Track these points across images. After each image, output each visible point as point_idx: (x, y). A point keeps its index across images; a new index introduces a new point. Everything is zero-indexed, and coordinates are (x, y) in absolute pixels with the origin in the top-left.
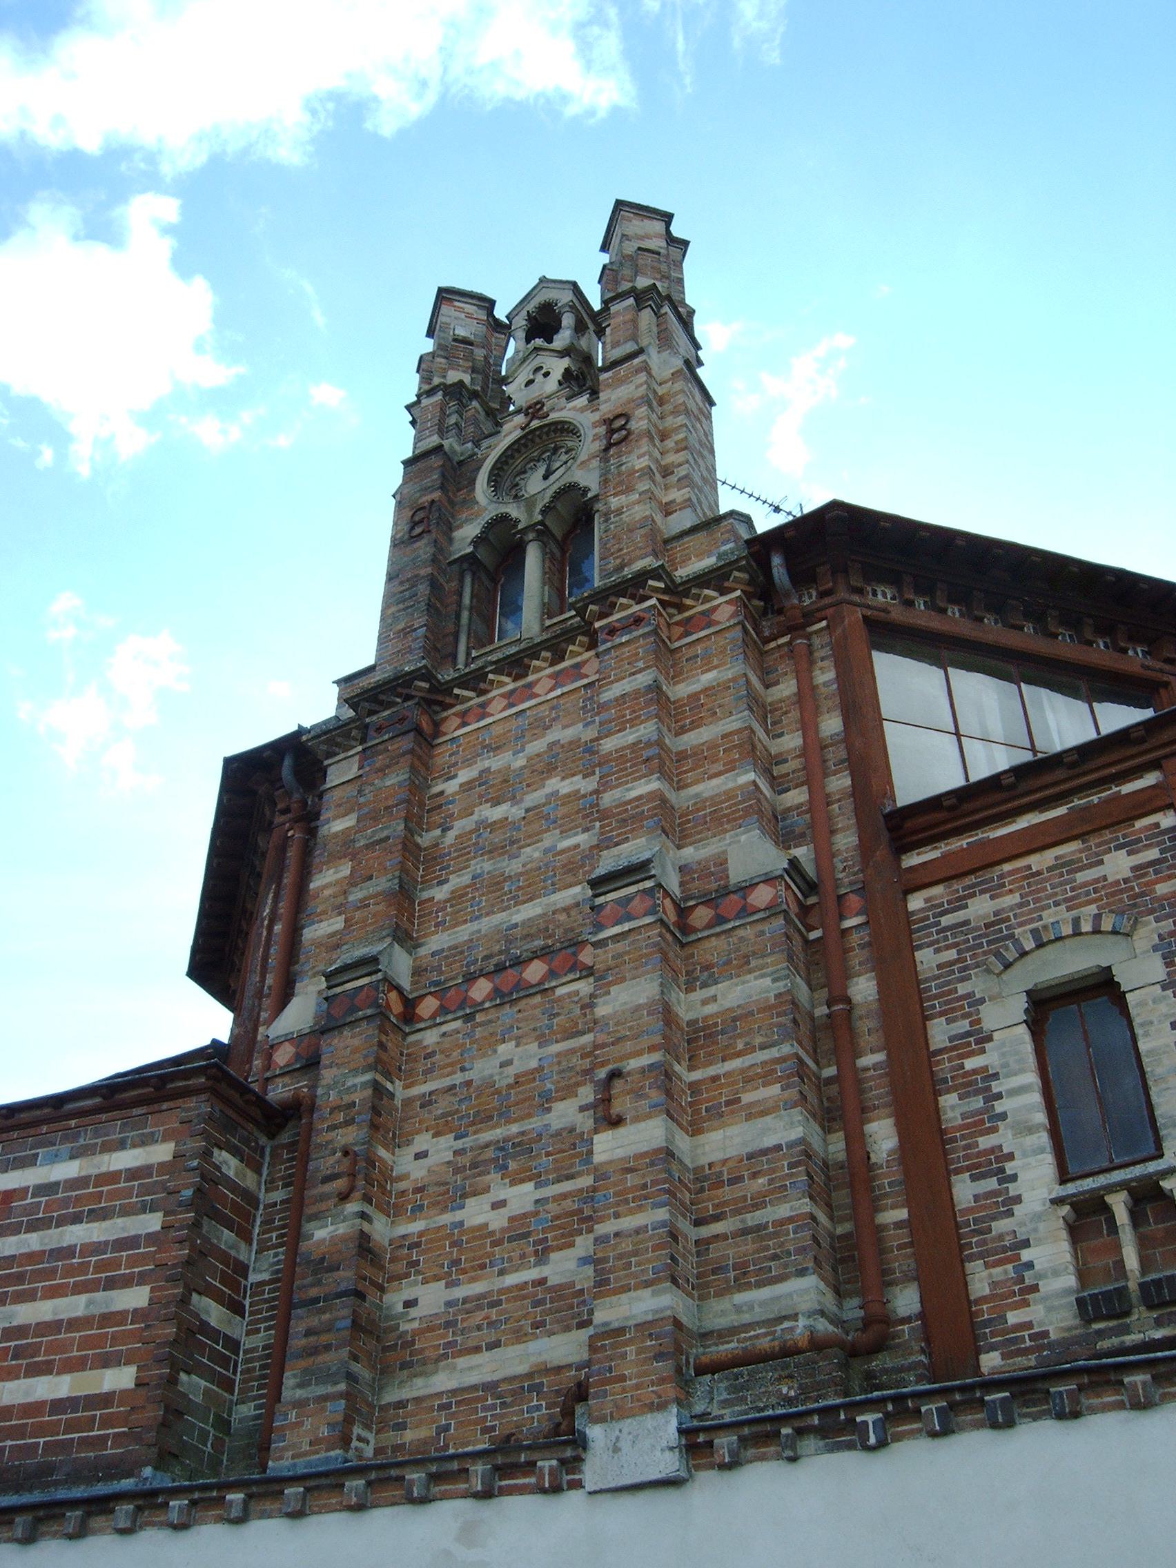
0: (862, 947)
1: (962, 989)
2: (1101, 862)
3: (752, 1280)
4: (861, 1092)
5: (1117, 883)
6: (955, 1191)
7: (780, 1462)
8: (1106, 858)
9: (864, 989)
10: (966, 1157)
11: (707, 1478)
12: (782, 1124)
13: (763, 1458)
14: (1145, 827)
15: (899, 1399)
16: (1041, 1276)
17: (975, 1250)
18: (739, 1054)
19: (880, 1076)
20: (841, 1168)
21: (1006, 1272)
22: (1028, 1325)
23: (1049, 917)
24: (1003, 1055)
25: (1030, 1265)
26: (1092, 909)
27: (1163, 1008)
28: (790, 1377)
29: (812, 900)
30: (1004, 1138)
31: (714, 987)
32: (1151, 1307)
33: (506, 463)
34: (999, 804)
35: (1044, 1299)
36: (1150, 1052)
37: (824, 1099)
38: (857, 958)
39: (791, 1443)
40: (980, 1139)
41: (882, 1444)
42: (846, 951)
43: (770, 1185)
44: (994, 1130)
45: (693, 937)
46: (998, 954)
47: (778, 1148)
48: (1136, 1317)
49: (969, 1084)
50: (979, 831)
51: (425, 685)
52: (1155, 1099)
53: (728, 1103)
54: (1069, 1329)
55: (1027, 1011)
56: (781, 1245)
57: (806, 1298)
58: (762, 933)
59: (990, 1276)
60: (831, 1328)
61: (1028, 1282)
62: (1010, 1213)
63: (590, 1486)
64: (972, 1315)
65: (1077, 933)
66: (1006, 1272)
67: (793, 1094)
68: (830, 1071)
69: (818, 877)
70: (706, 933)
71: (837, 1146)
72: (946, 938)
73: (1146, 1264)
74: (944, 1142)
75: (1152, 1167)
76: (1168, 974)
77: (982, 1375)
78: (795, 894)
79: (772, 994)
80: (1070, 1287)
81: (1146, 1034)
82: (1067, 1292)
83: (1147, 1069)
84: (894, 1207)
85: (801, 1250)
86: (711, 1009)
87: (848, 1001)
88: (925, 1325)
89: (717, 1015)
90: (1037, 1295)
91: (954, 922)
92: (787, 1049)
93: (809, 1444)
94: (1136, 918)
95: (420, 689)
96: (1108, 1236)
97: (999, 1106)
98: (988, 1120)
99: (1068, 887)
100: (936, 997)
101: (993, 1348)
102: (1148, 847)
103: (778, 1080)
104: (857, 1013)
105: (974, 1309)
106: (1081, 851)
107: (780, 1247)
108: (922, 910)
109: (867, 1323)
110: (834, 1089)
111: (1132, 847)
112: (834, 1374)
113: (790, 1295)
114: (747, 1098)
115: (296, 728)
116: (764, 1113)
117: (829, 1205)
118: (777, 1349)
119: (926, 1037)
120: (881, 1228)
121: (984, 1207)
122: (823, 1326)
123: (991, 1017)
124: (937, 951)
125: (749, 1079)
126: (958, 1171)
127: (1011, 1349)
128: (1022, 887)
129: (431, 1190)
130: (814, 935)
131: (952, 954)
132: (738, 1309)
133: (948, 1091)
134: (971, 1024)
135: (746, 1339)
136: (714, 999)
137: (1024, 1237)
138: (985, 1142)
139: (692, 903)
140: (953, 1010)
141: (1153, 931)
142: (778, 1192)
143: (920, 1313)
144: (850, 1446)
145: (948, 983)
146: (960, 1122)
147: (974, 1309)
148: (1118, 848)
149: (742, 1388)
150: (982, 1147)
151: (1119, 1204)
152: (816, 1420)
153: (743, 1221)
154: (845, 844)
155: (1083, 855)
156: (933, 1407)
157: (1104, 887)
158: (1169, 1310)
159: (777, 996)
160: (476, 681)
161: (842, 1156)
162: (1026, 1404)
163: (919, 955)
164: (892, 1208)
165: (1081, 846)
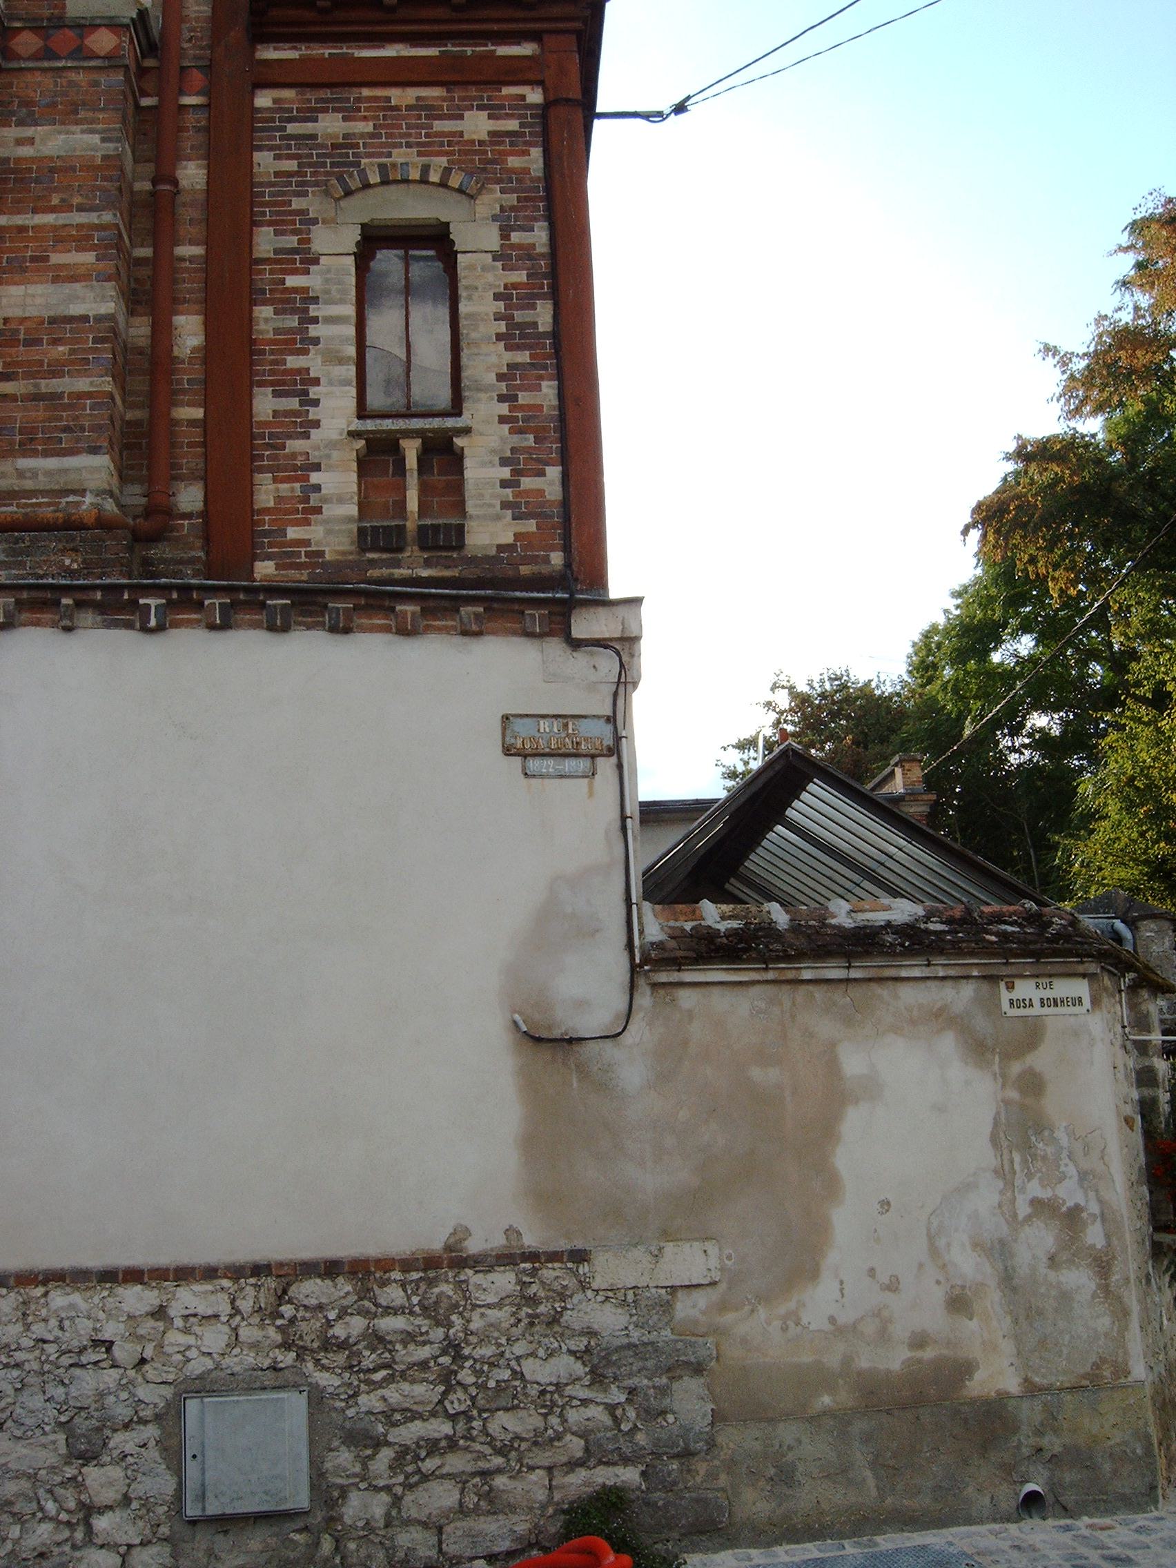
0: (198, 130)
1: (296, 204)
2: (461, 117)
3: (40, 448)
4: (175, 281)
5: (473, 142)
6: (255, 402)
7: (55, 629)
8: (467, 114)
9: (192, 174)
10: (272, 372)
12: (92, 295)
13: (37, 624)
14: (511, 95)
15: (187, 589)
16: (326, 500)
17: (265, 463)
18: (53, 210)
19: (196, 270)
20: (140, 354)
21: (293, 490)
22: (306, 543)
23: (400, 156)
24: (327, 281)
25: (317, 488)
26: (443, 161)
27: (490, 277)
28: (75, 550)
29: (150, 63)
30: (313, 362)
31: (33, 128)
32: (423, 548)
34: (379, 23)
35: (326, 522)
36: (470, 316)
37: (132, 280)
38: (190, 140)
39: (69, 613)
40: (289, 358)
41: (160, 628)
42: (181, 129)
43: (70, 355)
44: (305, 352)
45: (15, 65)
46: (340, 179)
47: (85, 318)
48: (409, 554)
49: (288, 301)
50: (344, 46)
52: (464, 360)
53: (34, 259)
54: (343, 553)
55: (358, 243)
56: (76, 418)
57: (96, 476)
58: (96, 84)
59: (277, 490)
60: (115, 509)
61: (312, 503)
62: (306, 436)
64: (254, 523)
65: (424, 181)
66: (293, 490)
67: (108, 266)
68: (145, 252)
69: (161, 39)
70: (31, 64)
71: (139, 330)
72: (289, 147)
73: (423, 509)
74: (252, 353)
75: (450, 423)
76: (502, 245)
77: (255, 581)
78: (135, 48)
79: (99, 154)
80: (353, 517)
81: (470, 298)
82: (349, 519)
83: (464, 331)
84: (191, 404)
85: (95, 428)
86: (26, 151)
87: (175, 183)
88: (206, 524)
89: (33, 159)
90: (320, 516)
91: (300, 132)
92: (107, 217)
93: (88, 617)
94: (483, 185)
96: (393, 475)
97: (314, 331)
98: (301, 342)
99: (423, 132)
100: (268, 204)
101: (268, 557)
102: (509, 116)
103: (93, 248)
104: (181, 199)
105: (255, 518)
106: (443, 99)
107: (73, 420)
108: (268, 109)
109: (149, 512)
110: (145, 272)
111: (495, 112)
112: (121, 555)
113: (78, 470)
114: (56, 258)
116: (74, 279)
117: (123, 388)
118: (61, 521)
119: (251, 242)
120: (176, 423)
121: (281, 424)
122: (110, 506)
123: (321, 240)
124: (277, 157)
125: (61, 238)
126: (262, 384)
127: (286, 560)
128: (377, 118)
130: (146, 102)
131: (292, 165)
132: (21, 474)
133: (265, 303)
134: (300, 241)
135: (26, 505)
136: (31, 141)
137: (316, 461)
138: (293, 362)
139: (18, 25)
140: (283, 222)
141: (496, 200)
142: (79, 365)
143: (203, 511)
144: (129, 625)
145: (284, 194)
146: (271, 335)
147: (255, 518)
148: (480, 108)
149: (21, 552)
150: (289, 365)
151: (411, 450)
152: (99, 595)
153: (36, 386)
154: (195, 12)
155: (445, 104)
156: (217, 602)
157: (458, 143)
158: (439, 554)
159: (105, 158)
161: (143, 342)
162: (303, 614)
163: (258, 156)
164: (188, 405)
165: (445, 94)
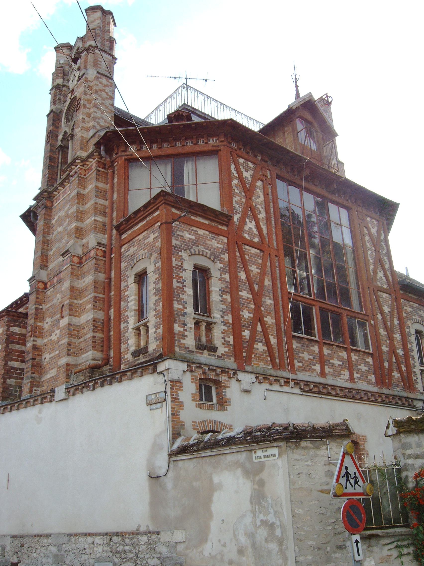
11: (71, 397)
33: (69, 110)
51: (46, 193)
63: (55, 401)
95: (46, 195)
115: (29, 207)
129: (48, 331)
160: (56, 189)
